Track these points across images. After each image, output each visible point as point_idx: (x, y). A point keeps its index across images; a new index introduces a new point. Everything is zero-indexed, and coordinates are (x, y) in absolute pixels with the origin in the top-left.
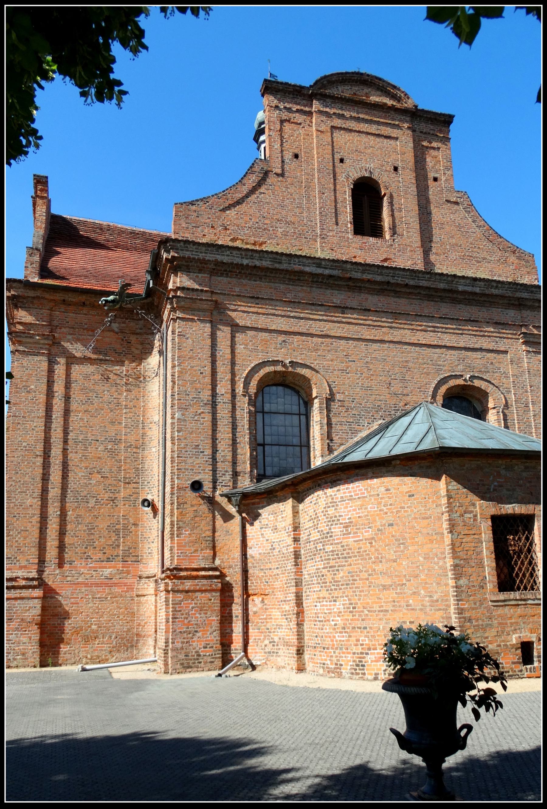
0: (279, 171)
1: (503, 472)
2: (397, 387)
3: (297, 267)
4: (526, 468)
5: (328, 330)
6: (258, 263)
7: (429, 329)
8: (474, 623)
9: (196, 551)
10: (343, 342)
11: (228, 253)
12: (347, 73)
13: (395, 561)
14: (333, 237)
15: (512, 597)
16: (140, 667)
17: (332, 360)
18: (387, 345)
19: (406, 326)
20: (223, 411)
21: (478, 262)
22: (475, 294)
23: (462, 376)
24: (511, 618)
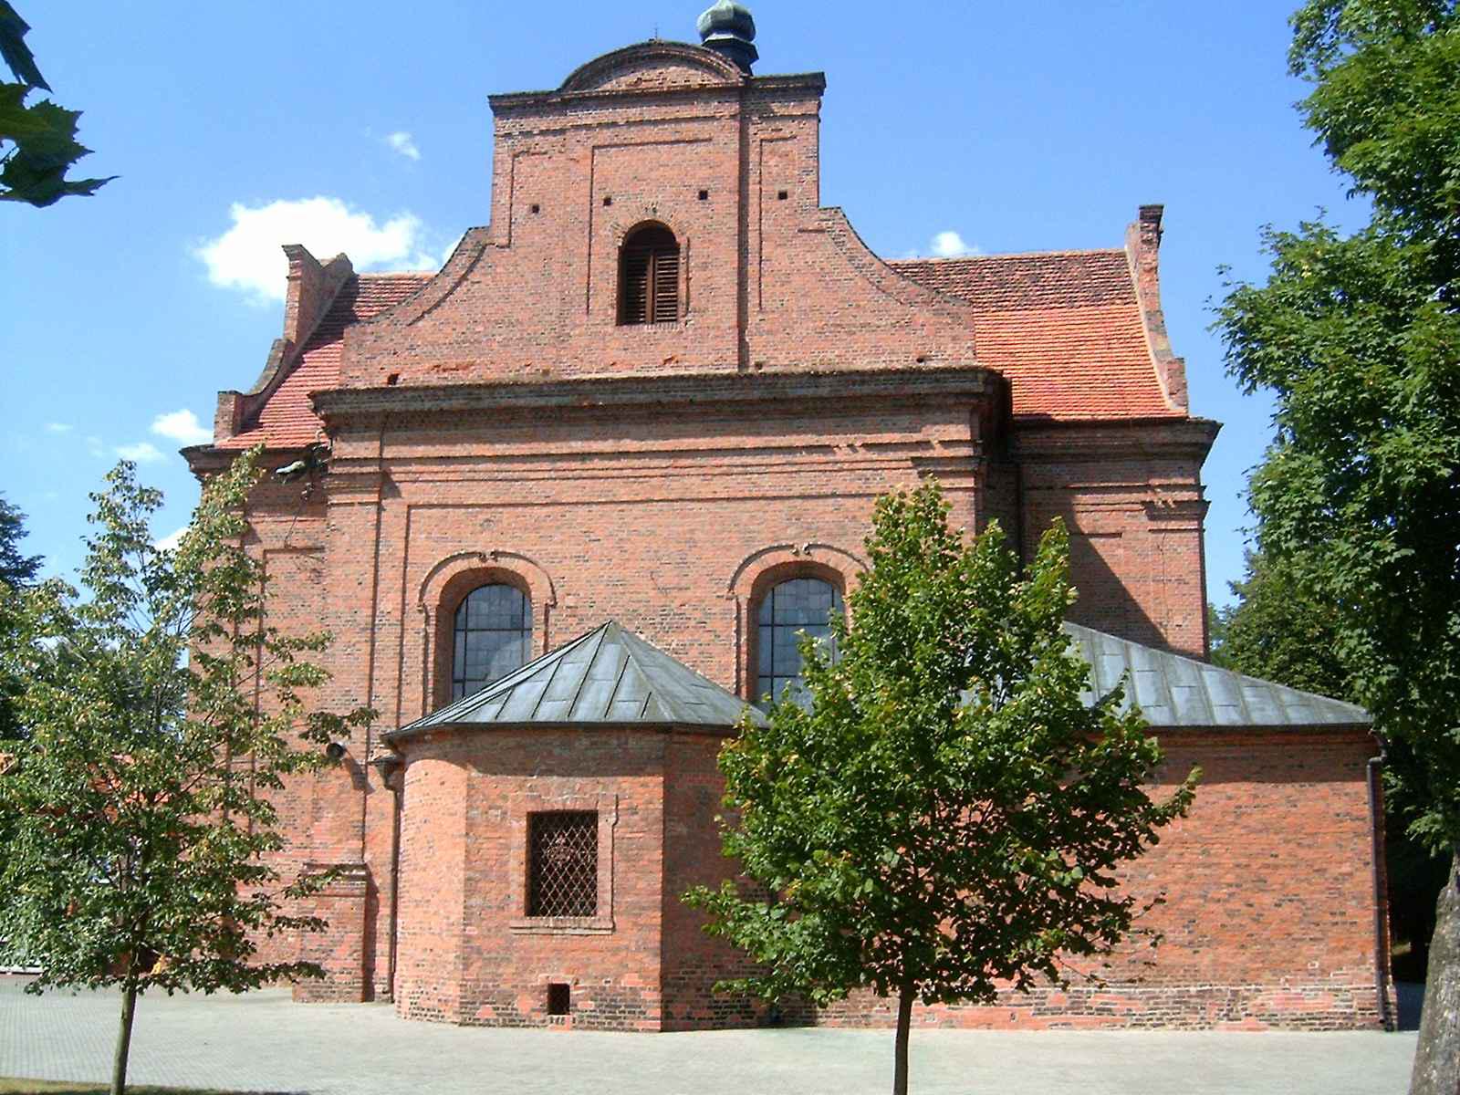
0: (504, 241)
1: (557, 751)
2: (668, 577)
3: (504, 402)
4: (592, 744)
5: (558, 493)
6: (445, 405)
7: (735, 470)
8: (486, 955)
9: (340, 841)
10: (582, 510)
11: (401, 397)
12: (622, 51)
14: (578, 338)
15: (542, 924)
17: (561, 542)
18: (656, 507)
19: (692, 471)
20: (387, 638)
21: (851, 333)
22: (822, 399)
23: (792, 546)
24: (540, 951)
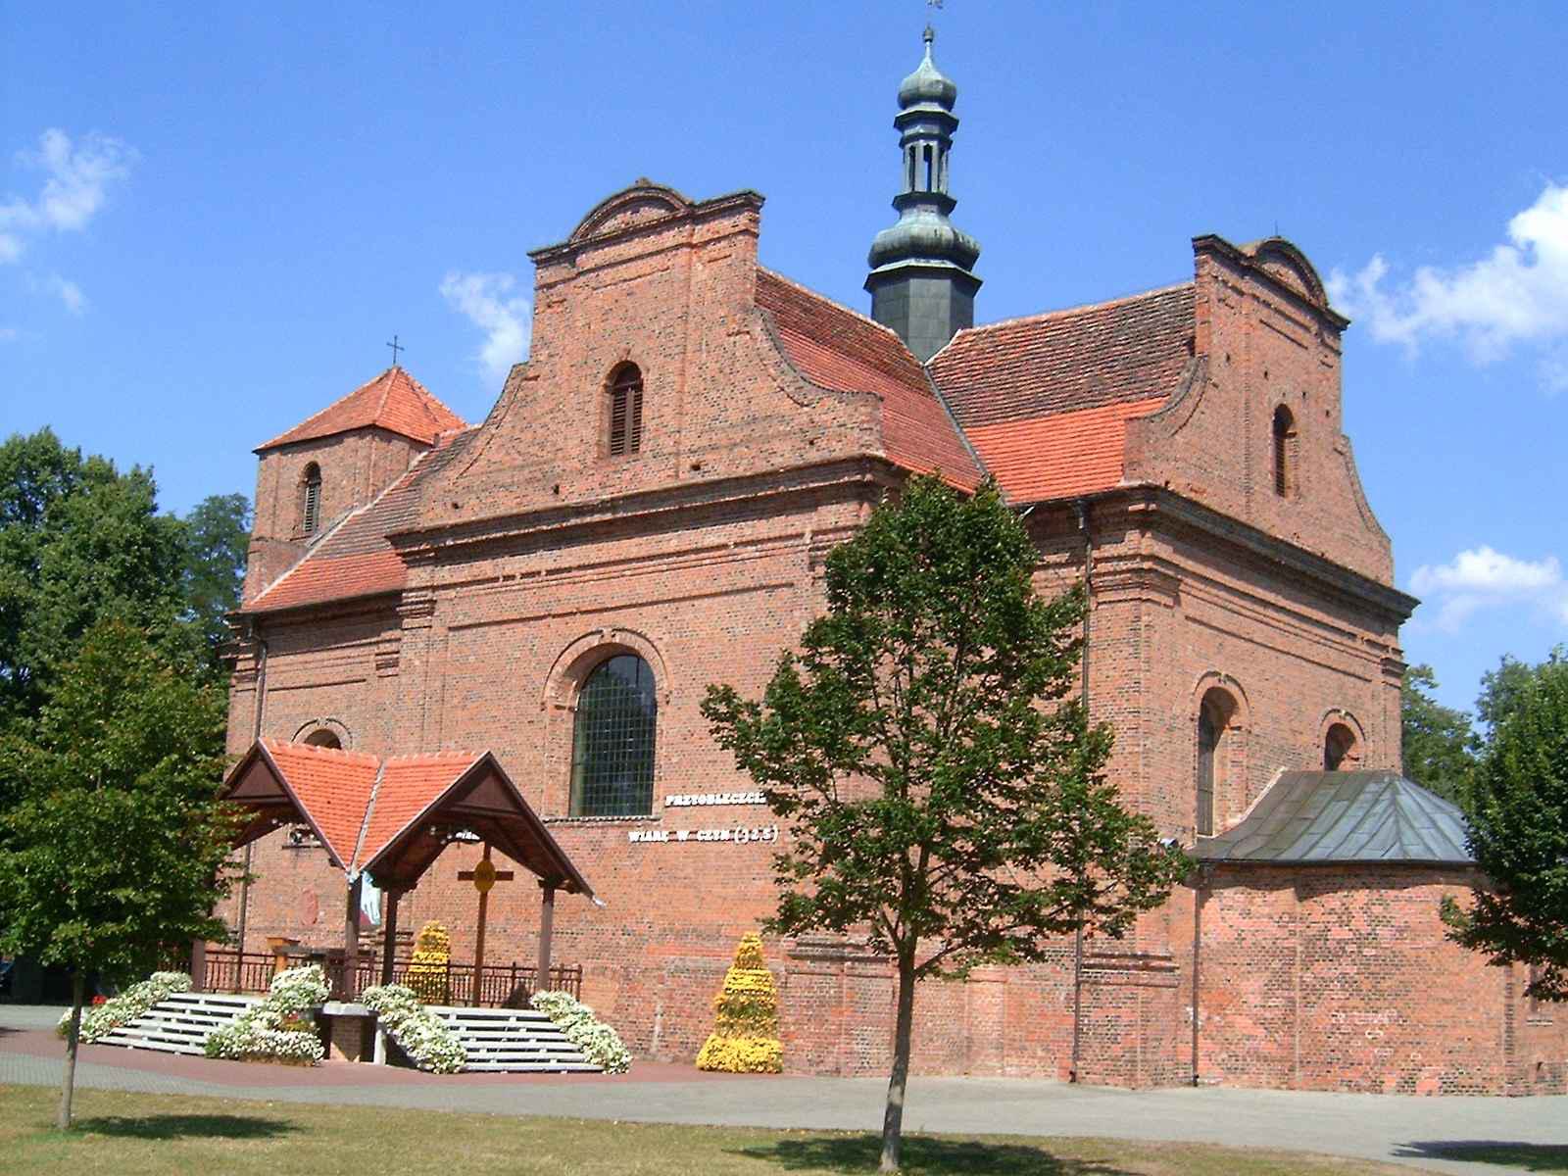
13: (1457, 974)
16: (367, 650)
